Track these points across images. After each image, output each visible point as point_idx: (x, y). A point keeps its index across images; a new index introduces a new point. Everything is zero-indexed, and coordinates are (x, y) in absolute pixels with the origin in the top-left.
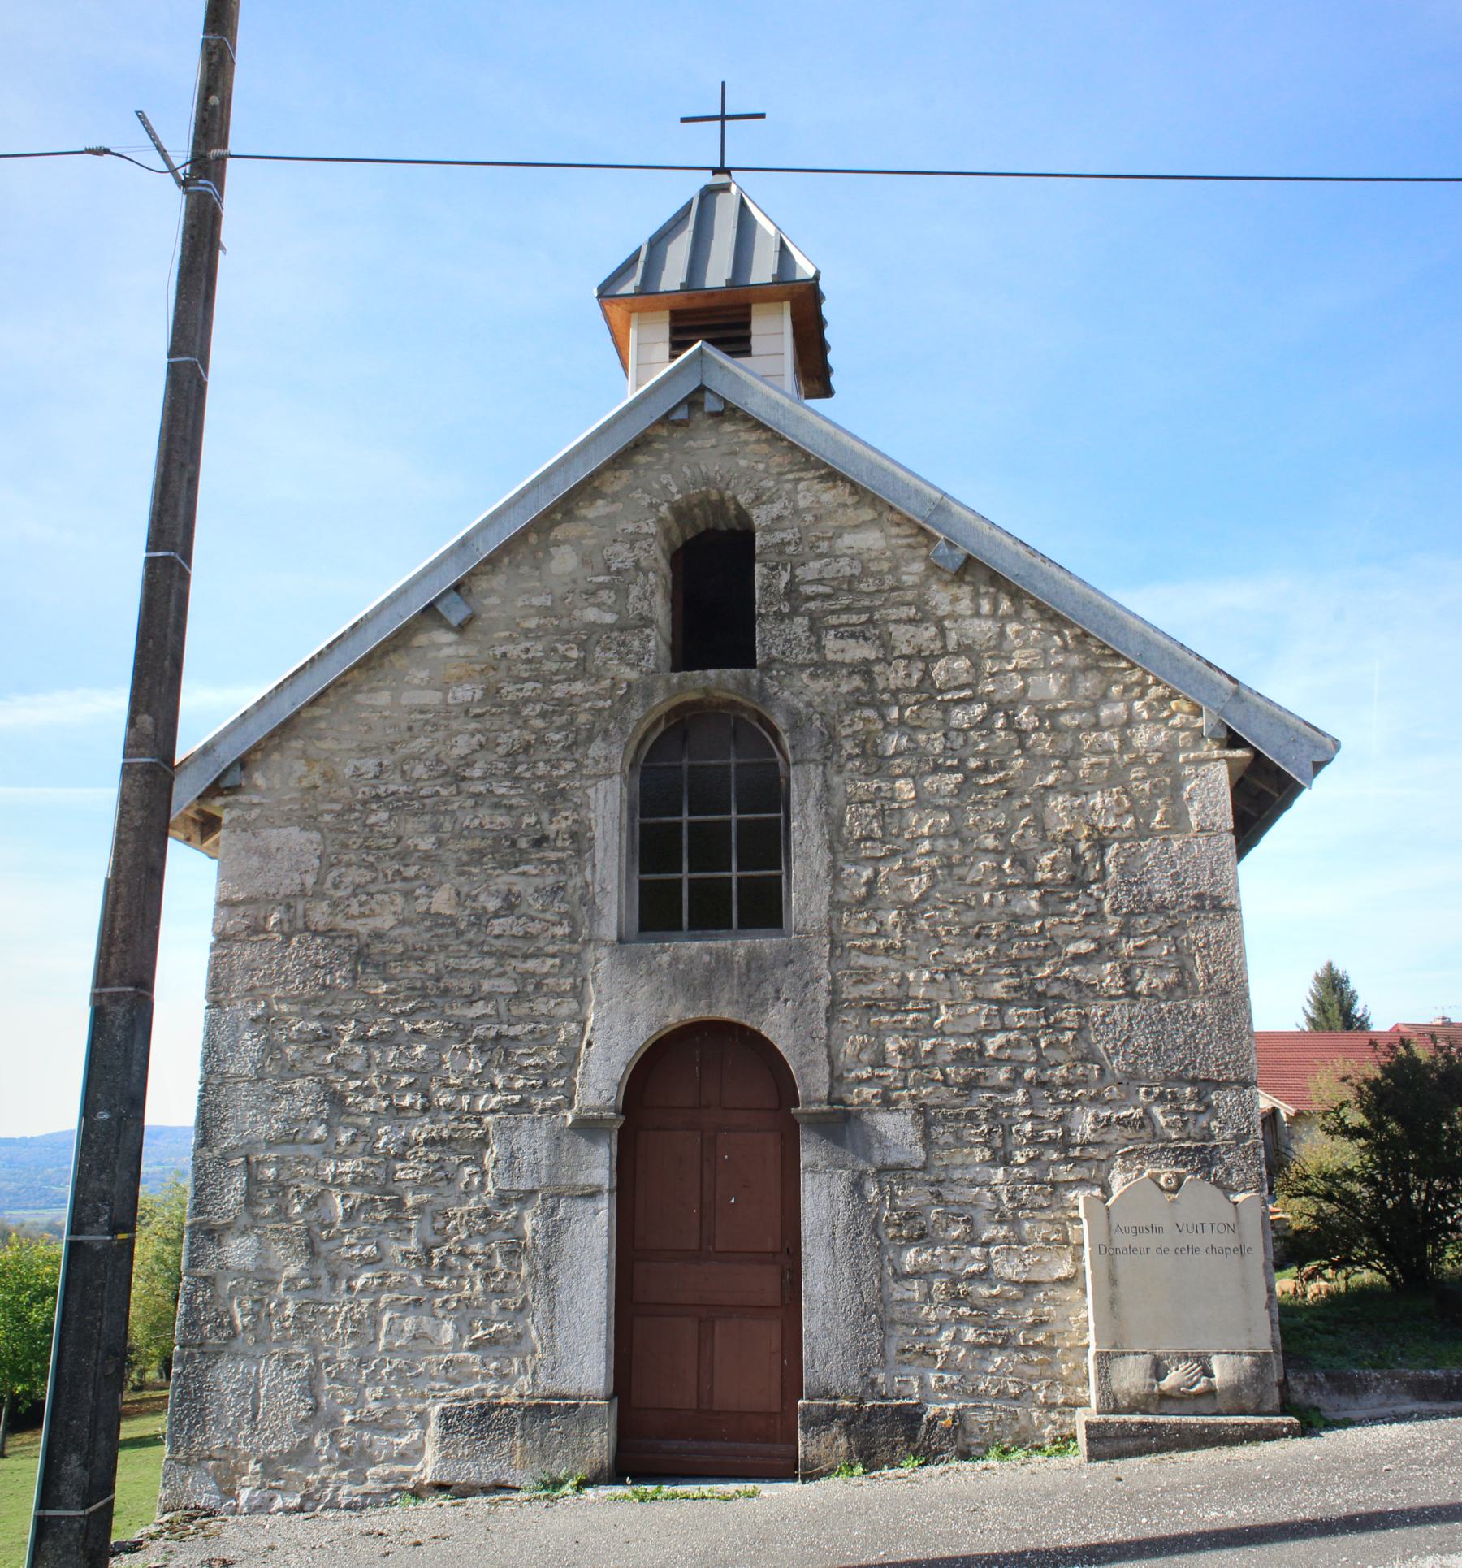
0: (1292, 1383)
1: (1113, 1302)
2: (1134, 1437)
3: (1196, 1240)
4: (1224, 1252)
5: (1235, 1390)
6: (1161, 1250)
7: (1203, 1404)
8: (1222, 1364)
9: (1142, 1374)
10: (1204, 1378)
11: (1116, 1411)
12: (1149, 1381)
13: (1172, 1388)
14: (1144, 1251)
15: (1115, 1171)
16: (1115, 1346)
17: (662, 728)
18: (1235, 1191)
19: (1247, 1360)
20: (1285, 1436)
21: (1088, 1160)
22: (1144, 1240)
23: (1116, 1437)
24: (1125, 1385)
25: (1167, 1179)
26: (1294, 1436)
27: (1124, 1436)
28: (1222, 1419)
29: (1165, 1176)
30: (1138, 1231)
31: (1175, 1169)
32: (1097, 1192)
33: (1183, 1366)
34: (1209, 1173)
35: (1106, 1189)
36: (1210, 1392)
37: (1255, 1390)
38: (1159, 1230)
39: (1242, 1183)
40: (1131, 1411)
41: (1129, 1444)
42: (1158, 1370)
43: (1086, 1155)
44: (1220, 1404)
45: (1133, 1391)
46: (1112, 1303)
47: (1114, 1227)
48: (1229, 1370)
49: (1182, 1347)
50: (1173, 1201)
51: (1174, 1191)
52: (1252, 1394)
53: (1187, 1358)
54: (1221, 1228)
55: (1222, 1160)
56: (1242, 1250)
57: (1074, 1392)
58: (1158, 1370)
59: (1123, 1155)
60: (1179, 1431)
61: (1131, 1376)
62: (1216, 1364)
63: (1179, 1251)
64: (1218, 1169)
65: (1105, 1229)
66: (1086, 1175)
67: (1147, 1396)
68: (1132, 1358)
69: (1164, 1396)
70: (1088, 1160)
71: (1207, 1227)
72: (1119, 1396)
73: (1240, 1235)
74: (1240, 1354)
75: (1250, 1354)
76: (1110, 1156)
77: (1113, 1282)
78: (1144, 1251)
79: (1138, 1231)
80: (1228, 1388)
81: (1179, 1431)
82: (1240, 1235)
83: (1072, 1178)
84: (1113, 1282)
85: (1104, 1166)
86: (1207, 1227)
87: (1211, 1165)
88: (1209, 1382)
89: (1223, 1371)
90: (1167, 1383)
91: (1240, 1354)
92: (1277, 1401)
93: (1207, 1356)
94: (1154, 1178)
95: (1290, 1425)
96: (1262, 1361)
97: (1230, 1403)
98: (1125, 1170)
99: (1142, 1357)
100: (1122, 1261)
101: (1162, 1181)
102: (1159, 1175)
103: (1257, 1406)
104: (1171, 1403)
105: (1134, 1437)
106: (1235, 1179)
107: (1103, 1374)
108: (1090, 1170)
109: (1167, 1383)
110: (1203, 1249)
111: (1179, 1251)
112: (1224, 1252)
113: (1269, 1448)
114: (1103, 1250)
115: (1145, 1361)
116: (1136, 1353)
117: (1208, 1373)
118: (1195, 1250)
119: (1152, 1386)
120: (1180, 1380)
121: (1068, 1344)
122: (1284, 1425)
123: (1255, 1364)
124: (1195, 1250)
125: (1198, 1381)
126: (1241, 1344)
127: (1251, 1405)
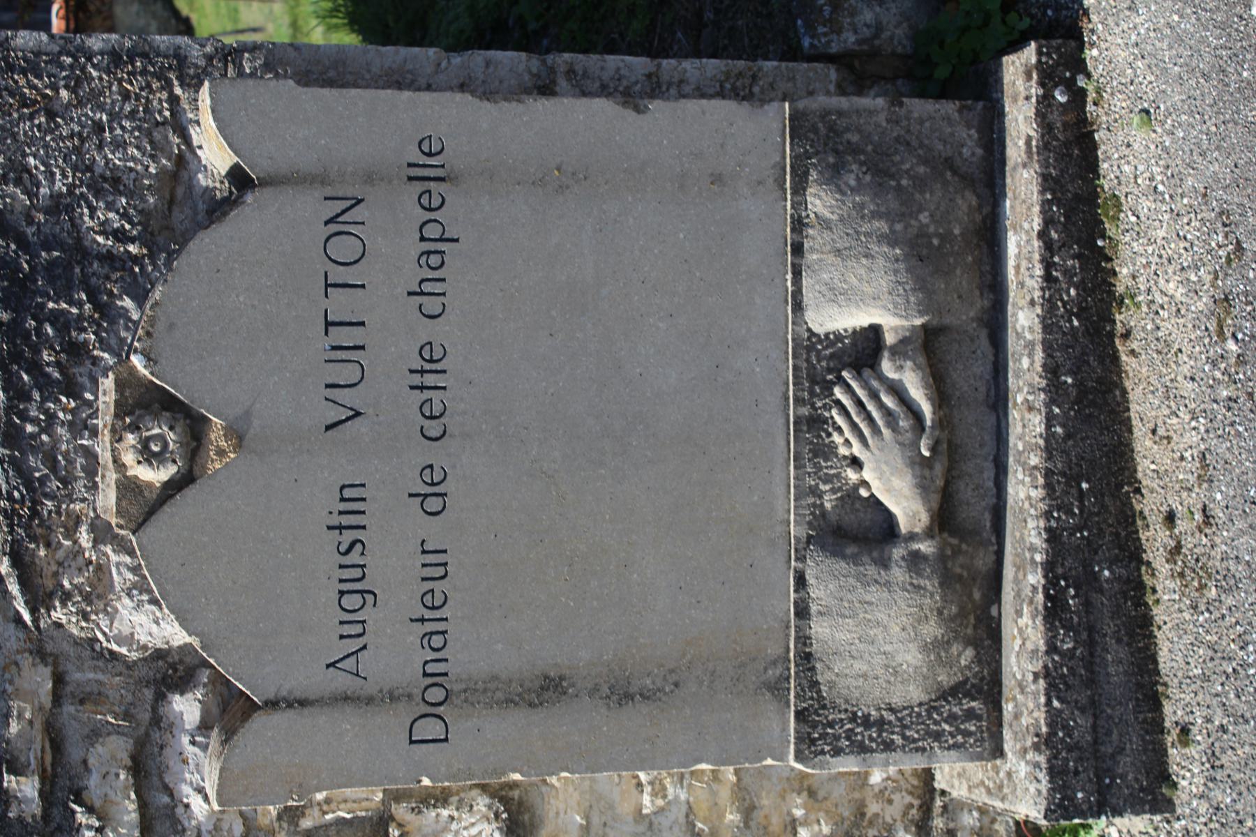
0: (850, 38)
1: (622, 693)
2: (1091, 640)
3: (393, 341)
4: (435, 246)
5: (923, 259)
6: (431, 494)
7: (968, 376)
8: (838, 295)
9: (874, 594)
10: (887, 367)
11: (988, 687)
12: (898, 574)
13: (923, 487)
14: (435, 562)
15: (104, 630)
16: (777, 689)
17: (71, 16)
18: (185, 161)
19: (819, 202)
20: (1079, 97)
21: (56, 741)
22: (392, 564)
23: (1093, 708)
24: (911, 657)
25: (147, 456)
26: (1080, 66)
27: (1091, 682)
28: (1024, 320)
29: (128, 462)
30: (356, 588)
31: (104, 420)
32: (187, 708)
33: (844, 442)
34: (108, 258)
35: (172, 671)
36: (929, 346)
37: (921, 184)
38: (351, 499)
39: (150, 129)
40: (988, 638)
41: (1115, 658)
42: (858, 532)
43: (35, 751)
44: (965, 313)
45: (932, 630)
46: (629, 697)
47: (340, 681)
48: (855, 273)
49: (782, 442)
50: (237, 435)
51: (195, 427)
52: (932, 197)
53: (815, 424)
54: (344, 248)
55: (60, 206)
56: (429, 175)
57: (883, 795)
58: (858, 532)
59: (39, 599)
60: (1072, 479)
61: (879, 638)
62: (836, 318)
63: (434, 425)
64: (99, 222)
65: (348, 722)
66: (116, 748)
67: (947, 580)
68: (819, 629)
69: (944, 519)
70: (56, 741)
71: (341, 305)
72: (945, 678)
73: (369, 178)
74: (799, 225)
75: (800, 188)
76: (41, 654)
77: (549, 689)
78: (435, 562)
79: (356, 588)
80: (922, 285)
81: (1072, 479)
82: (369, 178)
83: (129, 810)
84: (549, 689)
85: (82, 676)
86: (341, 305)
87: (80, 250)
88: (898, 351)
89: (858, 298)
90: (904, 503)
91: (799, 225)
92: (949, 107)
93: (809, 344)
94: (144, 507)
95: (1047, 76)
96: (822, 147)
97: (963, 279)
98: (97, 595)
99: (818, 592)
100: (468, 657)
101: (155, 476)
102: (129, 487)
103: (967, 181)
104: (965, 491)
105: (1091, 640)
106: (132, 157)
107: (872, 731)
108: (95, 734)
109: (904, 503)
110: (426, 331)
111: (434, 425)
112: (435, 246)
113: (1130, 159)
114: (431, 728)
115: (827, 581)
116: (802, 612)
117: (865, 349)
118: (431, 360)
119: (915, 559)
120: (897, 457)
121: (732, 817)
122: (1045, 101)
123: (833, 175)
124: (431, 360)
125: (897, 391)
126: (765, 215)
127: (966, 202)
